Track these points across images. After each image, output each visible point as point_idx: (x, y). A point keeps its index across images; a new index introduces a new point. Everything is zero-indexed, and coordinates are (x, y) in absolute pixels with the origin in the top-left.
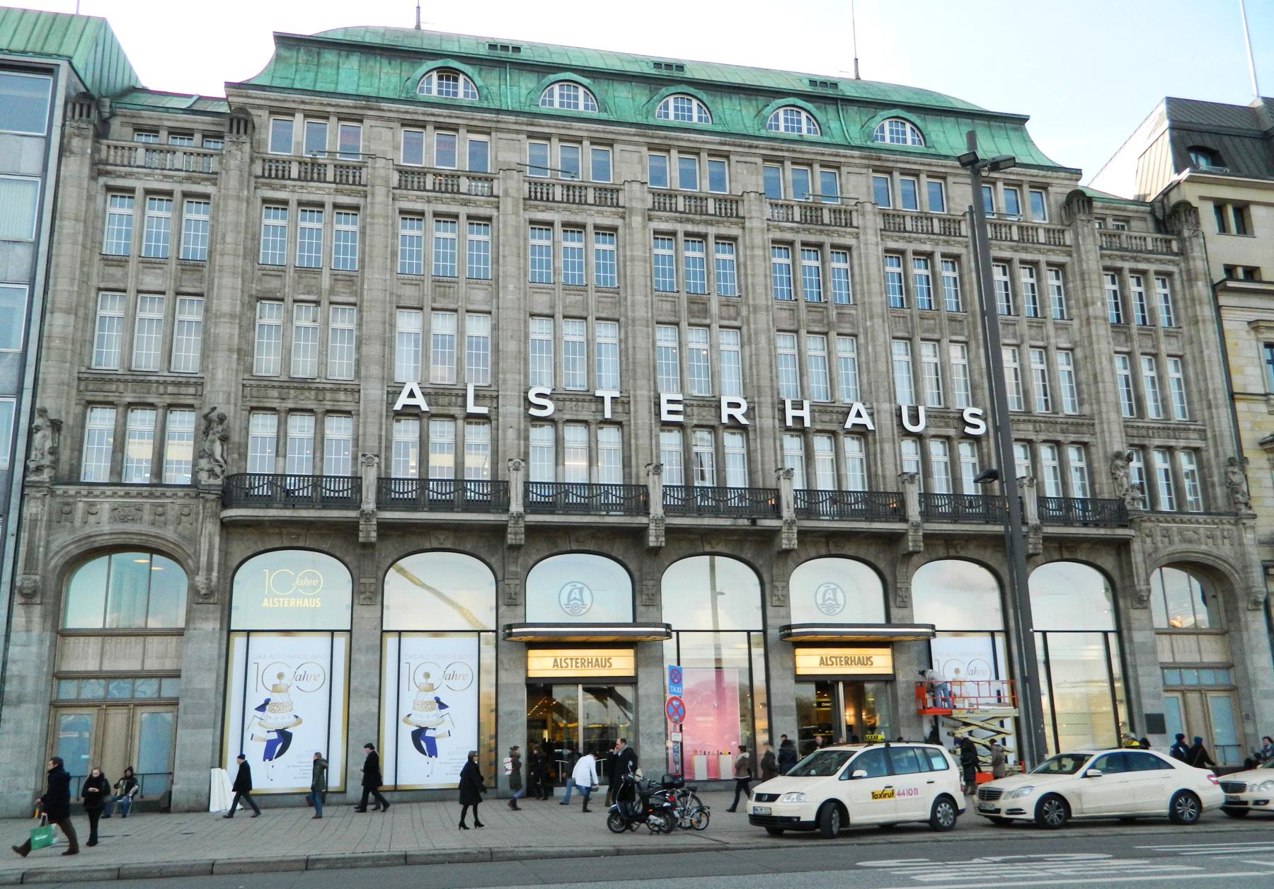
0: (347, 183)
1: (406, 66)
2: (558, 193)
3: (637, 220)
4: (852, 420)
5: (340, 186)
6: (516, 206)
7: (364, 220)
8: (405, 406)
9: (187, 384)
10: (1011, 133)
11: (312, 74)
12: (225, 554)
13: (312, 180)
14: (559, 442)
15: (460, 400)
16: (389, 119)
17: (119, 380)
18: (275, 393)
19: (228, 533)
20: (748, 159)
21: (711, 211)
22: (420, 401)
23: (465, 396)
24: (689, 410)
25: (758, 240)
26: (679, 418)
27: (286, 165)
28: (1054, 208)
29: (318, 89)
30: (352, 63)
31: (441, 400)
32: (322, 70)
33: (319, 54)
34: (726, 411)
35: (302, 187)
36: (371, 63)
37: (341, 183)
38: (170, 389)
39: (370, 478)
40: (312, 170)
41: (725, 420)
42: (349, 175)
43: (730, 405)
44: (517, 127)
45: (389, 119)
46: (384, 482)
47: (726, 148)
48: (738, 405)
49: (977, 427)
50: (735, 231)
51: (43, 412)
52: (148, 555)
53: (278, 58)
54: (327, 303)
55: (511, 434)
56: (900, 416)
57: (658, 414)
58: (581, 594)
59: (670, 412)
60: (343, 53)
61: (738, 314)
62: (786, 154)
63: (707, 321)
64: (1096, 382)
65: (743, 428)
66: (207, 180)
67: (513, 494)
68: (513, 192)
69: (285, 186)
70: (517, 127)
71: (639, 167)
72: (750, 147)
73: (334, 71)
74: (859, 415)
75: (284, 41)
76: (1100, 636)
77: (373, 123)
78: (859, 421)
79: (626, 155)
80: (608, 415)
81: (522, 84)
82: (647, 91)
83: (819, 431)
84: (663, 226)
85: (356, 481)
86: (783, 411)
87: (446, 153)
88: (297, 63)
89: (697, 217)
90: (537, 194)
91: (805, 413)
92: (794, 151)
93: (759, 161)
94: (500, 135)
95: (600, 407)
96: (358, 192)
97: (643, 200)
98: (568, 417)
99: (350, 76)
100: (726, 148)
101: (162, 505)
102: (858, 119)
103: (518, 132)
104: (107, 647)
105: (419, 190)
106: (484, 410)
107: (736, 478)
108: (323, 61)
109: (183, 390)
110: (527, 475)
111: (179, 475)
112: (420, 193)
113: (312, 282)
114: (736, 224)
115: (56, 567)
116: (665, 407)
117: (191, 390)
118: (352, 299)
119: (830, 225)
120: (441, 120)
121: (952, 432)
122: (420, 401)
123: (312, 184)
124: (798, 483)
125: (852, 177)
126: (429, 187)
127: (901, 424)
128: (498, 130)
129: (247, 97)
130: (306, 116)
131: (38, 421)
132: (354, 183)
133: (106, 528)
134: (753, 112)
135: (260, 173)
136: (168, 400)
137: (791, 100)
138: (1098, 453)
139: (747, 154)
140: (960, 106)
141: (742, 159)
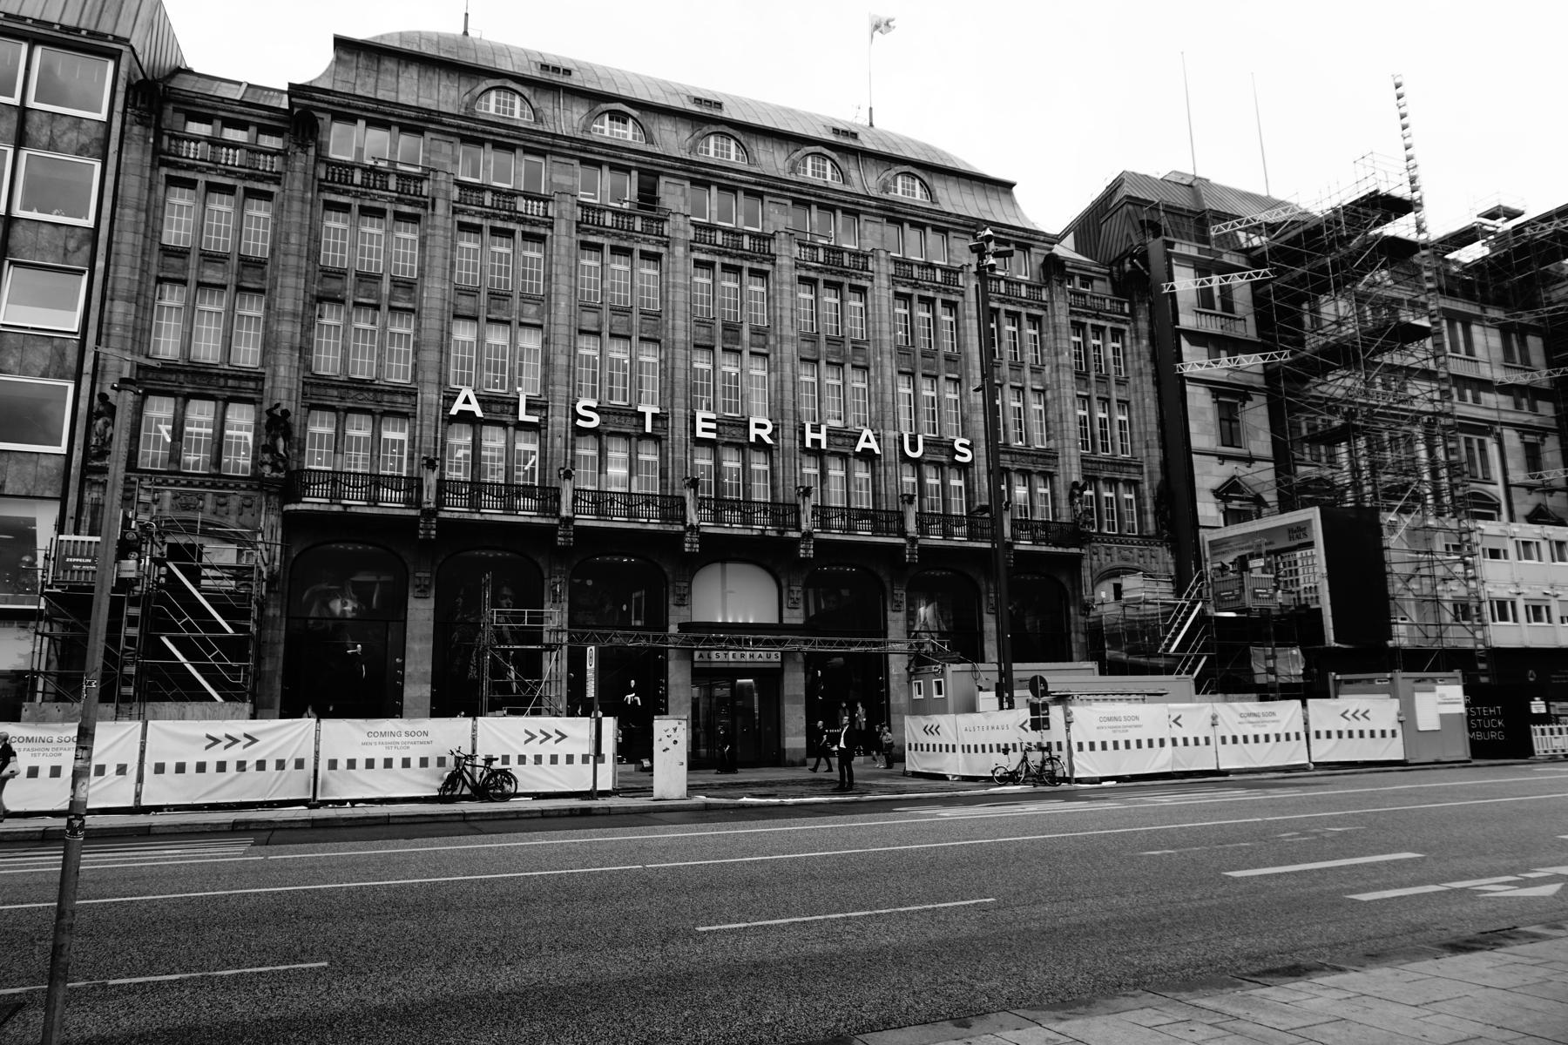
1: (463, 81)
3: (680, 250)
4: (861, 445)
6: (569, 228)
15: (511, 409)
23: (517, 405)
26: (713, 436)
28: (1035, 268)
34: (753, 431)
36: (430, 74)
38: (230, 382)
43: (758, 426)
48: (764, 427)
49: (964, 455)
50: (767, 267)
53: (338, 60)
57: (694, 431)
59: (704, 430)
61: (767, 343)
67: (563, 499)
71: (682, 200)
75: (341, 43)
77: (434, 136)
78: (867, 446)
86: (803, 433)
91: (823, 437)
93: (789, 203)
97: (686, 232)
101: (224, 495)
103: (572, 157)
106: (535, 419)
109: (244, 384)
111: (240, 461)
116: (700, 425)
117: (252, 385)
118: (410, 306)
121: (944, 459)
128: (552, 153)
137: (818, 149)
138: (1060, 482)
140: (963, 167)
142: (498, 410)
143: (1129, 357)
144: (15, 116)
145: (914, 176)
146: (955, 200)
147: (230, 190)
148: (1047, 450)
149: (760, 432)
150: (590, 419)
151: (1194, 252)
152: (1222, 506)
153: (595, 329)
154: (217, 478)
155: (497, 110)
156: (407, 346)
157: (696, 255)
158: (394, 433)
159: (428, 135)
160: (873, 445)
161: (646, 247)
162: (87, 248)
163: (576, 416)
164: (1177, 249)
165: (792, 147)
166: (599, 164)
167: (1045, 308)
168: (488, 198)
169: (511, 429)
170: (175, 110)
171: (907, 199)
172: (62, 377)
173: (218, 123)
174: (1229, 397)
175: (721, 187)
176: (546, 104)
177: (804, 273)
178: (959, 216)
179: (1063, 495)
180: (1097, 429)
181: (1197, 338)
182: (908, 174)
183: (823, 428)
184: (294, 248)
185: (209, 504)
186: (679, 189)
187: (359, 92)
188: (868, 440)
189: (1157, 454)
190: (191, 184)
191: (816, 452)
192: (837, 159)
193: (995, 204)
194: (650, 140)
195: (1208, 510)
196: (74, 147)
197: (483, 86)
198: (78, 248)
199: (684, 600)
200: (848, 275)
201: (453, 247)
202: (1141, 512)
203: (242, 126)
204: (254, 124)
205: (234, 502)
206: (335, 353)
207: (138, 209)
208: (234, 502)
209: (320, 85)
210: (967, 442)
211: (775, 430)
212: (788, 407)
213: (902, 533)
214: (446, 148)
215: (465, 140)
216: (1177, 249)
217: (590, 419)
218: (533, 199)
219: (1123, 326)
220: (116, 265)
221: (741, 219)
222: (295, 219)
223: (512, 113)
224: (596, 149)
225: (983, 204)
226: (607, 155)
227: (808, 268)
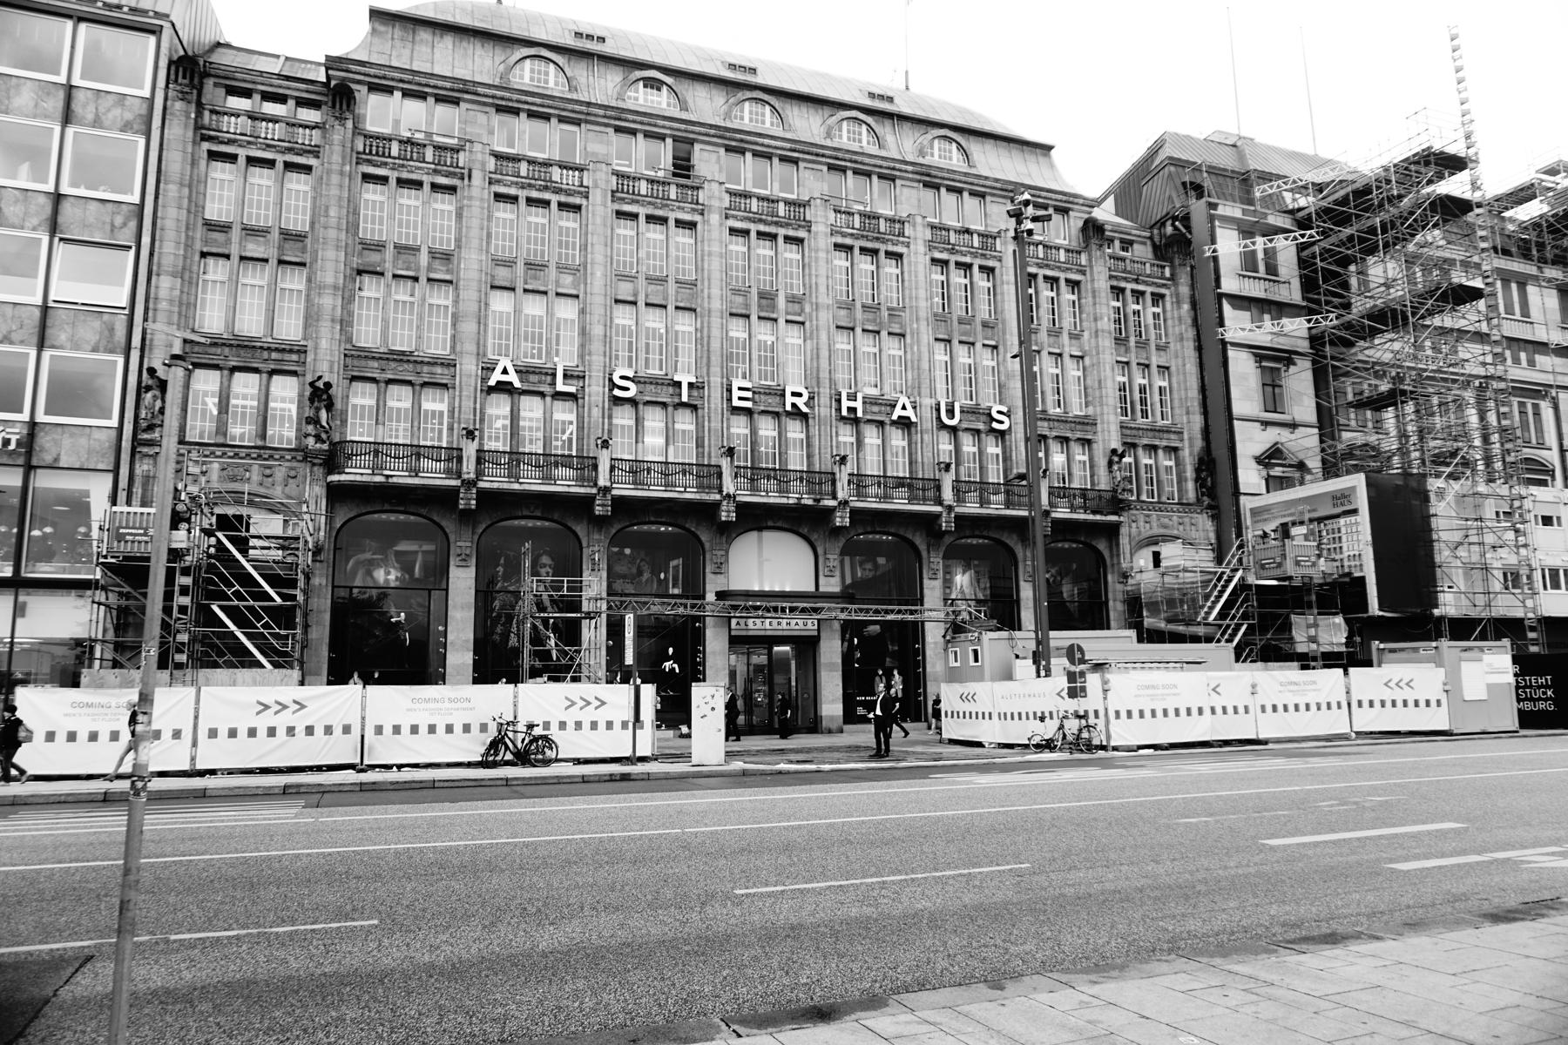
1: (498, 50)
3: (715, 218)
4: (898, 412)
9: (291, 351)
16: (485, 104)
22: (513, 378)
26: (748, 404)
34: (789, 400)
36: (465, 44)
38: (274, 355)
41: (788, 408)
43: (794, 394)
45: (485, 104)
48: (800, 395)
50: (801, 234)
51: (152, 371)
56: (938, 410)
57: (730, 400)
61: (802, 310)
64: (1100, 387)
67: (600, 468)
68: (602, 184)
69: (386, 164)
71: (717, 167)
74: (904, 408)
75: (377, 15)
78: (904, 413)
83: (869, 421)
86: (839, 401)
91: (858, 405)
93: (825, 168)
97: (721, 199)
101: (269, 467)
103: (607, 125)
106: (572, 389)
108: (417, 38)
109: (287, 357)
116: (736, 394)
117: (294, 357)
118: (448, 277)
121: (981, 426)
127: (939, 418)
128: (587, 122)
143: (1170, 322)
144: (61, 94)
145: (951, 140)
146: (992, 163)
148: (1086, 416)
149: (796, 400)
150: (627, 389)
151: (1238, 214)
152: (1264, 473)
154: (263, 451)
155: (532, 79)
160: (909, 413)
162: (133, 224)
163: (613, 385)
164: (1221, 211)
165: (827, 111)
167: (1083, 273)
170: (216, 85)
171: (943, 163)
172: (111, 351)
173: (257, 97)
174: (1273, 360)
175: (756, 154)
176: (579, 71)
177: (840, 240)
178: (997, 180)
179: (1102, 462)
180: (1137, 396)
181: (1240, 301)
183: (860, 396)
184: (333, 221)
186: (714, 156)
188: (904, 408)
189: (1197, 421)
192: (963, 143)
194: (684, 108)
195: (1250, 477)
196: (119, 124)
198: (125, 224)
199: (720, 569)
200: (885, 241)
201: (489, 218)
202: (1181, 480)
203: (282, 99)
205: (280, 473)
207: (182, 185)
208: (280, 473)
210: (1005, 409)
211: (811, 398)
212: (824, 375)
213: (939, 502)
214: (482, 118)
215: (500, 109)
216: (1221, 211)
217: (627, 389)
219: (1163, 291)
221: (776, 186)
222: (334, 191)
223: (546, 82)
224: (630, 117)
226: (642, 123)
227: (844, 235)
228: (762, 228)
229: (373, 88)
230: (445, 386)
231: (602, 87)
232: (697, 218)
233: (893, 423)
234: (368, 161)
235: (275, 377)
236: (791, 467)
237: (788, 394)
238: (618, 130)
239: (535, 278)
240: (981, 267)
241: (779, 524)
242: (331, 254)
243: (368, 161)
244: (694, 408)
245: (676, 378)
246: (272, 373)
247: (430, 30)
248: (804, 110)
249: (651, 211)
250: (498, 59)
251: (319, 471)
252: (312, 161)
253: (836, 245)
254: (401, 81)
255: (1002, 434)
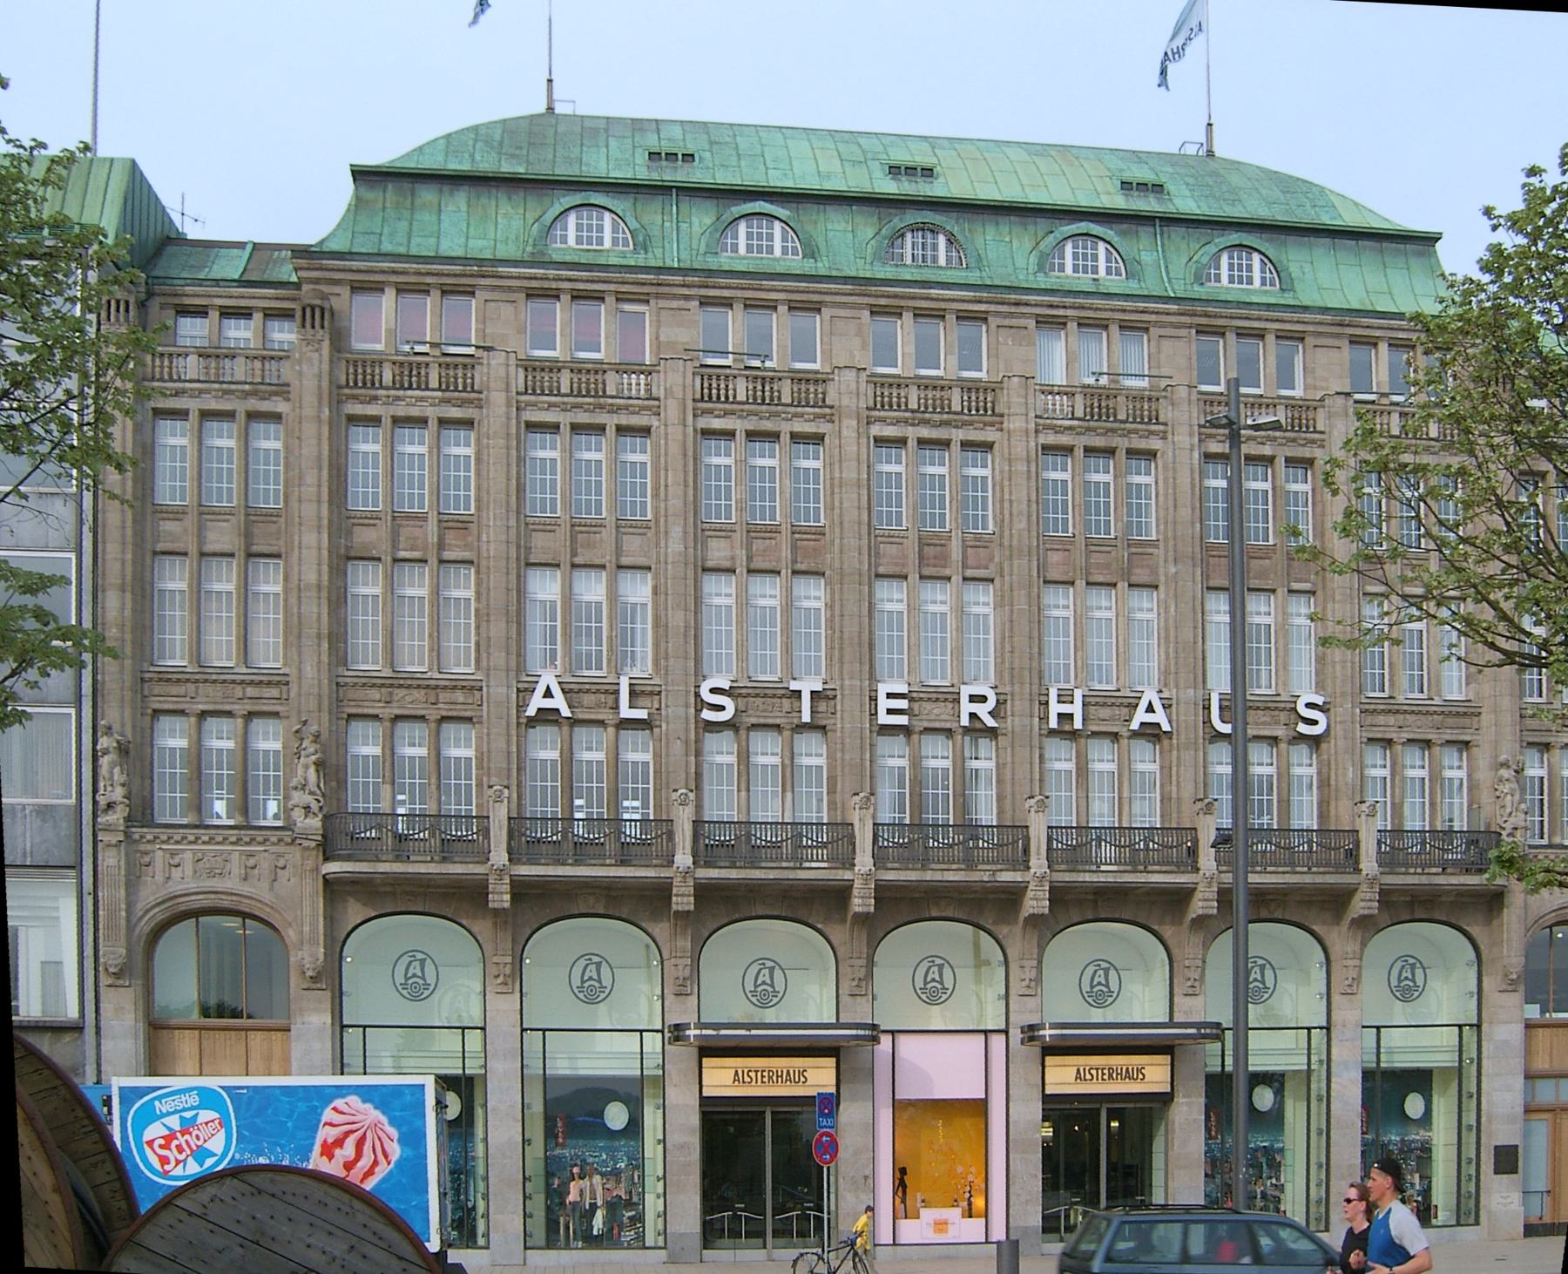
0: (456, 390)
1: (532, 202)
2: (741, 389)
3: (849, 426)
4: (1141, 716)
5: (447, 394)
7: (478, 441)
8: (539, 710)
10: (1413, 261)
11: (404, 225)
12: (330, 920)
13: (410, 388)
14: (744, 757)
17: (188, 680)
18: (375, 694)
19: (333, 892)
20: (1014, 322)
21: (956, 407)
22: (559, 702)
23: (617, 692)
24: (916, 706)
25: (1019, 448)
26: (902, 720)
27: (599, 377)
29: (413, 252)
30: (458, 203)
31: (588, 699)
32: (418, 216)
33: (413, 195)
34: (966, 707)
35: (398, 398)
36: (484, 201)
37: (447, 390)
38: (250, 691)
39: (499, 817)
40: (410, 373)
41: (965, 721)
42: (458, 373)
43: (973, 699)
44: (686, 291)
45: (510, 289)
46: (516, 824)
47: (983, 307)
50: (990, 435)
52: (240, 920)
53: (358, 204)
54: (435, 561)
55: (678, 747)
56: (1207, 708)
57: (874, 714)
58: (598, 971)
59: (890, 711)
60: (446, 188)
62: (1069, 312)
63: (947, 572)
65: (992, 733)
66: (276, 394)
67: (678, 838)
69: (376, 398)
70: (686, 291)
71: (857, 341)
72: (1017, 304)
73: (434, 218)
75: (361, 175)
76: (1003, 1027)
77: (489, 295)
78: (1150, 718)
79: (840, 324)
80: (806, 718)
81: (695, 220)
82: (875, 219)
83: (1095, 734)
84: (890, 431)
85: (665, 826)
87: (926, 355)
88: (384, 208)
89: (936, 417)
90: (712, 388)
91: (1076, 709)
92: (1082, 307)
93: (1032, 323)
94: (662, 303)
95: (796, 704)
96: (824, 416)
98: (754, 720)
99: (455, 228)
100: (983, 307)
101: (251, 855)
102: (1184, 246)
103: (687, 298)
104: (252, 1044)
105: (551, 394)
106: (641, 714)
107: (1305, 816)
108: (418, 202)
110: (699, 807)
112: (553, 399)
113: (417, 532)
114: (992, 424)
115: (140, 936)
116: (884, 704)
117: (275, 692)
118: (466, 555)
119: (1126, 422)
120: (581, 286)
121: (1280, 732)
122: (559, 702)
123: (409, 393)
124: (1383, 821)
125: (1166, 343)
126: (565, 389)
127: (1207, 721)
128: (658, 296)
129: (321, 269)
130: (399, 291)
131: (104, 742)
132: (464, 390)
133: (192, 886)
134: (1028, 245)
135: (343, 383)
136: (249, 707)
137: (1084, 226)
139: (1011, 315)
140: (1376, 224)
141: (1007, 322)
142: (589, 706)
146: (1330, 281)
147: (229, 415)
153: (727, 564)
155: (579, 240)
156: (467, 617)
157: (876, 430)
158: (461, 748)
159: (827, 312)
160: (1159, 717)
161: (799, 426)
163: (701, 704)
165: (1043, 224)
166: (728, 303)
168: (565, 380)
169: (1283, 746)
171: (1236, 291)
175: (918, 314)
176: (654, 214)
177: (1050, 438)
178: (1325, 310)
182: (922, 228)
183: (1078, 694)
185: (236, 866)
187: (387, 247)
188: (1150, 709)
190: (182, 414)
191: (1065, 731)
192: (1115, 240)
193: (1397, 278)
194: (1287, 285)
197: (557, 209)
200: (615, 410)
201: (521, 460)
204: (257, 309)
206: (375, 637)
209: (334, 246)
214: (507, 311)
215: (531, 295)
218: (630, 372)
220: (104, 542)
221: (953, 361)
223: (600, 241)
225: (1374, 279)
227: (1058, 430)
228: (925, 432)
229: (357, 288)
230: (470, 719)
231: (684, 236)
232: (823, 428)
233: (1135, 734)
234: (355, 397)
235: (444, 725)
236: (1408, 826)
237: (964, 699)
238: (705, 302)
239: (589, 546)
240: (1288, 460)
241: (949, 914)
242: (310, 538)
243: (355, 397)
244: (823, 729)
245: (794, 686)
246: (250, 716)
247: (1182, 230)
248: (1005, 229)
249: (752, 424)
250: (530, 217)
251: (315, 857)
252: (281, 406)
253: (1046, 449)
254: (394, 272)
255: (1315, 742)
